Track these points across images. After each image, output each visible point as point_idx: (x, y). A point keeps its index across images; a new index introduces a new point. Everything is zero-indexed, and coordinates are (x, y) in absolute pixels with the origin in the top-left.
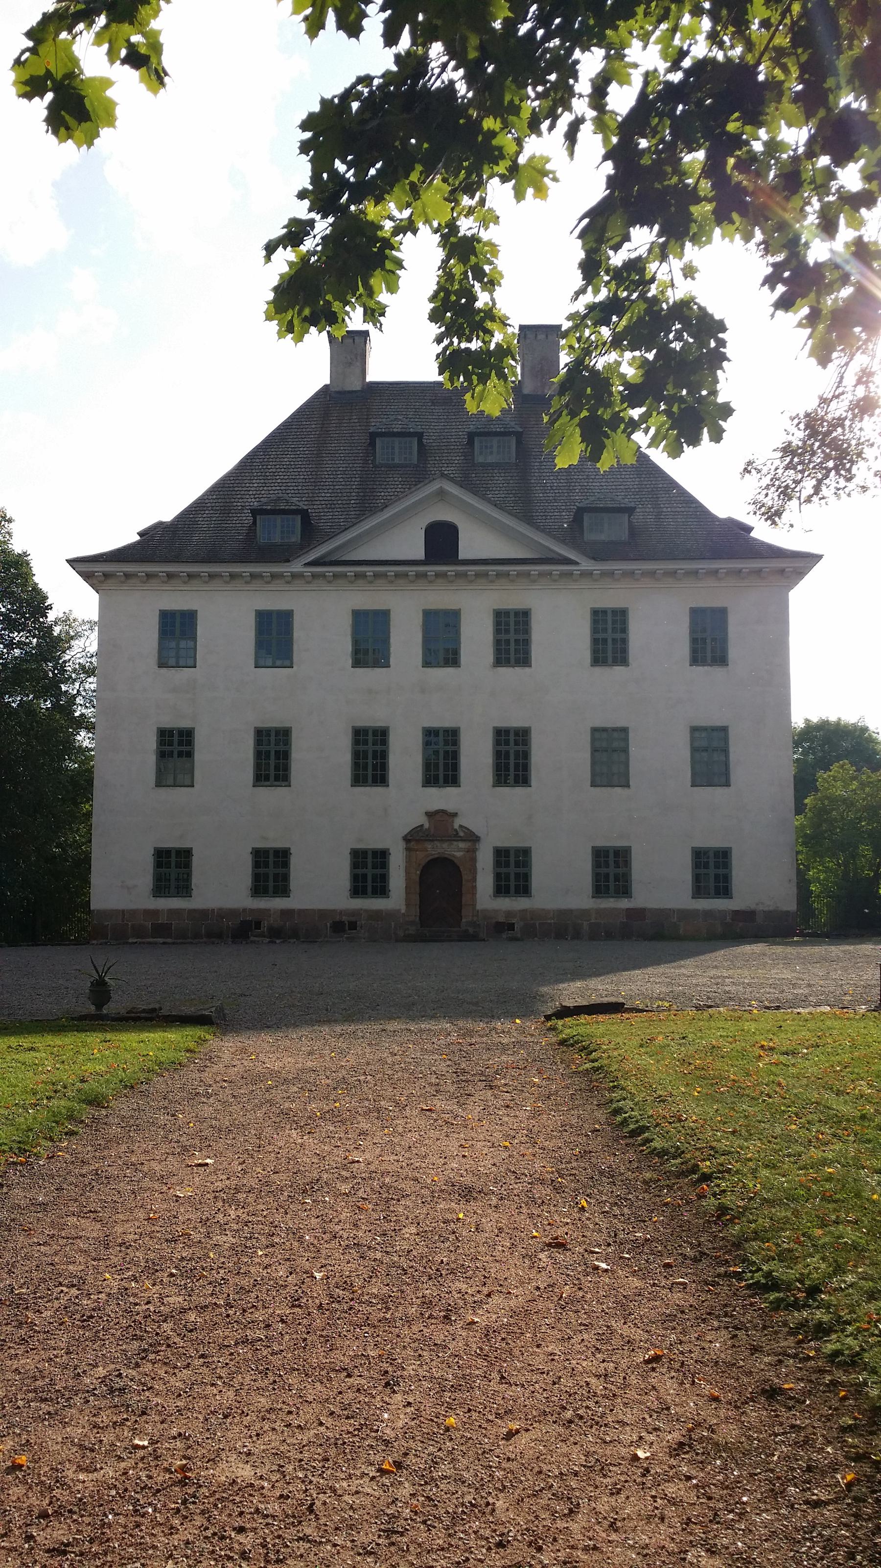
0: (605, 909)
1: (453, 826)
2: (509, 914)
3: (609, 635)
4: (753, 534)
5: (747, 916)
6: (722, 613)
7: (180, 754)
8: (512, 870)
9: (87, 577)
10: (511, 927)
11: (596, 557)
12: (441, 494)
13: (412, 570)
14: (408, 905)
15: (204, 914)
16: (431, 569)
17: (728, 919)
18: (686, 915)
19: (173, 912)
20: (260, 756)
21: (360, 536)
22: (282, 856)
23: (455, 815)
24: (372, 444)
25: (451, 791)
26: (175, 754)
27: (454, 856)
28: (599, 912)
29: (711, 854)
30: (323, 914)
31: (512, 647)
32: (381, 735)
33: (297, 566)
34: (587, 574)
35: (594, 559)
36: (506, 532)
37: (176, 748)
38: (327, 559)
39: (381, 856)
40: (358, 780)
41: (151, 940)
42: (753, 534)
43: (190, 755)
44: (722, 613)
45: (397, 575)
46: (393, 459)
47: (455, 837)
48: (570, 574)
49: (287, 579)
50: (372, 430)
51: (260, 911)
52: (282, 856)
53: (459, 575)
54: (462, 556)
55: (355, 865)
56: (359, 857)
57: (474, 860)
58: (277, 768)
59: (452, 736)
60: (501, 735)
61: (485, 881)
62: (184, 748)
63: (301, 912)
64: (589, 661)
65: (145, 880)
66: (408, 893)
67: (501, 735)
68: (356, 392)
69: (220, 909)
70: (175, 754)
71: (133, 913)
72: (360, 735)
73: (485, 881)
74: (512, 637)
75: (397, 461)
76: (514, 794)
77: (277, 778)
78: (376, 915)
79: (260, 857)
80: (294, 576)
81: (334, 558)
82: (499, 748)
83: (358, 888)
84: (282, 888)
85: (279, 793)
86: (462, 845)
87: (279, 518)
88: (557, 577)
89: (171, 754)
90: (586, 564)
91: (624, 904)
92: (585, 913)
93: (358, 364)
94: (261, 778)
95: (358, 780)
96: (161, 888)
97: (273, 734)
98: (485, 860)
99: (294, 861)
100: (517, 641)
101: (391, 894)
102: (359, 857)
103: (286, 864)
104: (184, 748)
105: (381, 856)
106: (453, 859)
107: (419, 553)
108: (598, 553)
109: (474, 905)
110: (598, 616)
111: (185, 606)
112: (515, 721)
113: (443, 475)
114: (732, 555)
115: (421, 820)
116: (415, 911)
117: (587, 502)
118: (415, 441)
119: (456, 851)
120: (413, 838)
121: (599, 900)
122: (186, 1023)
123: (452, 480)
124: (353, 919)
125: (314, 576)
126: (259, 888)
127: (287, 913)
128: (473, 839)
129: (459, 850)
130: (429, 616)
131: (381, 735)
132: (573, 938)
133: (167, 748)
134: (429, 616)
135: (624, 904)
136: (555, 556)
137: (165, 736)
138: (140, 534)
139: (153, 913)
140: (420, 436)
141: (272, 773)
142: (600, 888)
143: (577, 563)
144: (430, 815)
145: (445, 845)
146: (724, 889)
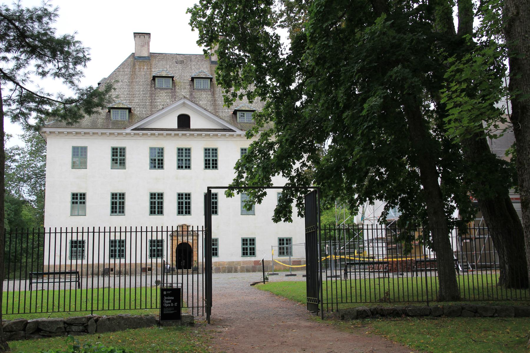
0: (246, 261)
3: (211, 158)
7: (81, 203)
12: (184, 104)
13: (173, 133)
16: (180, 133)
21: (153, 119)
22: (252, 241)
25: (187, 217)
26: (79, 203)
31: (211, 162)
32: (161, 196)
33: (128, 130)
35: (242, 130)
37: (79, 200)
38: (139, 128)
39: (160, 243)
40: (152, 212)
46: (162, 86)
50: (154, 75)
52: (252, 241)
54: (192, 126)
62: (82, 201)
64: (277, 254)
68: (145, 57)
70: (79, 203)
74: (184, 158)
75: (164, 87)
80: (127, 134)
84: (122, 254)
87: (120, 111)
89: (77, 203)
91: (253, 259)
92: (238, 263)
93: (146, 46)
95: (152, 212)
100: (186, 160)
104: (82, 201)
105: (160, 243)
107: (175, 126)
111: (83, 145)
117: (239, 107)
118: (171, 79)
121: (244, 258)
130: (180, 151)
131: (161, 196)
132: (235, 272)
133: (75, 201)
134: (180, 151)
136: (227, 128)
137: (75, 196)
140: (173, 77)
143: (235, 131)
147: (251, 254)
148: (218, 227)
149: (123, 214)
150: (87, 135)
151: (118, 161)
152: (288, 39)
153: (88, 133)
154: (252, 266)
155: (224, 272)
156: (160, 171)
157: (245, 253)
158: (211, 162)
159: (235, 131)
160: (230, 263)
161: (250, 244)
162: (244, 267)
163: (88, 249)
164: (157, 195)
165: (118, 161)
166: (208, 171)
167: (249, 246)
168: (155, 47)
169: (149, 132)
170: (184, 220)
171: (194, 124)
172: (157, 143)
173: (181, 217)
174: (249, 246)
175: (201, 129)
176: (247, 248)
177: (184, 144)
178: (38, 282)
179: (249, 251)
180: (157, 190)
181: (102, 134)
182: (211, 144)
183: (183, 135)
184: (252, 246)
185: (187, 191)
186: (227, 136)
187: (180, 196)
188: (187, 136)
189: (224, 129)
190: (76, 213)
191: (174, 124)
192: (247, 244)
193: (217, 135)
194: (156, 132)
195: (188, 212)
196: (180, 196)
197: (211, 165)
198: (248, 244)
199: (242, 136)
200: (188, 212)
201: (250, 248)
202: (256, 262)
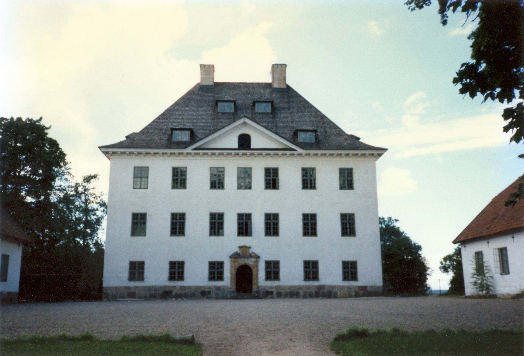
1: (249, 252)
2: (271, 287)
4: (360, 140)
5: (364, 288)
6: (313, 170)
7: (141, 223)
8: (216, 270)
9: (106, 153)
10: (272, 293)
11: (302, 148)
12: (245, 123)
13: (233, 152)
14: (231, 284)
15: (149, 288)
16: (241, 152)
17: (357, 289)
18: (341, 288)
19: (136, 288)
20: (240, 224)
22: (181, 264)
23: (250, 248)
24: (217, 104)
27: (250, 264)
28: (308, 287)
29: (137, 264)
30: (197, 288)
33: (189, 150)
34: (300, 155)
36: (271, 138)
38: (201, 147)
39: (221, 264)
41: (126, 299)
42: (360, 140)
43: (145, 223)
44: (313, 170)
45: (220, 154)
47: (251, 256)
48: (293, 154)
49: (168, 155)
51: (171, 287)
52: (181, 264)
53: (252, 154)
54: (253, 146)
55: (210, 268)
56: (212, 265)
57: (257, 266)
58: (180, 229)
59: (248, 216)
60: (268, 216)
61: (262, 274)
62: (142, 221)
63: (190, 287)
65: (126, 274)
66: (231, 278)
67: (268, 216)
69: (156, 286)
71: (120, 288)
72: (213, 216)
73: (262, 274)
76: (272, 239)
77: (180, 233)
78: (218, 288)
79: (172, 264)
80: (188, 154)
81: (203, 147)
82: (267, 221)
83: (212, 277)
84: (181, 277)
85: (180, 239)
86: (253, 260)
88: (264, 155)
90: (300, 151)
91: (316, 283)
92: (300, 287)
94: (306, 233)
96: (132, 277)
97: (178, 215)
98: (262, 266)
99: (146, 267)
101: (225, 279)
102: (212, 265)
103: (143, 268)
105: (221, 264)
106: (249, 265)
107: (236, 146)
108: (303, 146)
109: (257, 284)
110: (304, 170)
111: (145, 165)
112: (273, 211)
113: (245, 117)
114: (357, 148)
115: (236, 250)
116: (234, 288)
119: (250, 262)
120: (235, 256)
122: (495, 333)
123: (249, 118)
124: (209, 290)
125: (196, 154)
126: (172, 277)
127: (184, 288)
128: (258, 257)
129: (252, 262)
135: (316, 283)
136: (288, 148)
138: (127, 137)
139: (128, 288)
140: (235, 102)
141: (178, 231)
142: (307, 277)
144: (240, 247)
145: (246, 260)
146: (315, 277)
150: (148, 155)
151: (179, 181)
152: (469, 38)
153: (124, 153)
155: (305, 297)
160: (291, 287)
162: (307, 292)
165: (179, 181)
168: (219, 77)
169: (210, 152)
170: (244, 241)
171: (255, 143)
172: (217, 162)
182: (271, 163)
191: (234, 143)
193: (285, 154)
194: (217, 152)
199: (343, 156)
202: (360, 288)
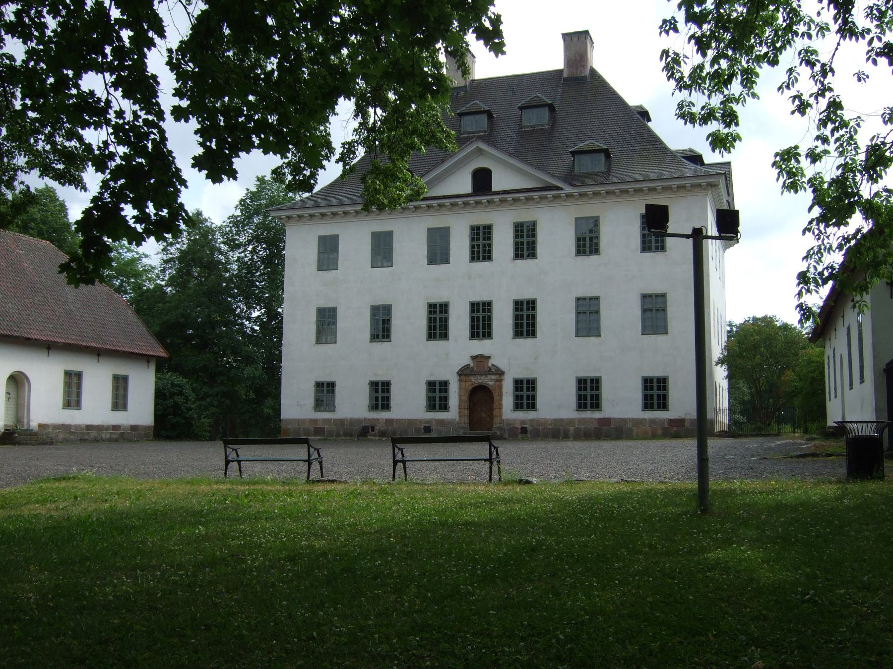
12: (479, 151)
22: (596, 383)
25: (487, 342)
28: (581, 421)
34: (569, 196)
39: (444, 385)
40: (431, 336)
51: (373, 419)
52: (596, 383)
54: (495, 188)
61: (508, 400)
68: (462, 87)
91: (597, 415)
92: (571, 422)
95: (431, 336)
105: (444, 385)
111: (333, 233)
127: (389, 422)
135: (597, 415)
143: (561, 189)
147: (592, 407)
148: (536, 358)
149: (387, 340)
154: (595, 428)
155: (654, 436)
156: (486, 264)
157: (648, 404)
158: (481, 249)
159: (561, 189)
161: (592, 389)
162: (580, 429)
163: (542, 395)
164: (525, 303)
166: (519, 262)
167: (525, 393)
170: (481, 347)
173: (476, 342)
174: (589, 393)
175: (516, 190)
176: (652, 396)
177: (481, 218)
178: (688, 448)
179: (525, 402)
180: (439, 297)
181: (607, 193)
182: (524, 215)
183: (540, 197)
184: (595, 392)
185: (485, 298)
186: (576, 197)
187: (474, 306)
188: (688, 188)
189: (547, 187)
190: (324, 341)
192: (585, 389)
195: (488, 335)
196: (474, 306)
197: (481, 255)
198: (655, 388)
200: (488, 335)
201: (659, 396)
202: (672, 422)
